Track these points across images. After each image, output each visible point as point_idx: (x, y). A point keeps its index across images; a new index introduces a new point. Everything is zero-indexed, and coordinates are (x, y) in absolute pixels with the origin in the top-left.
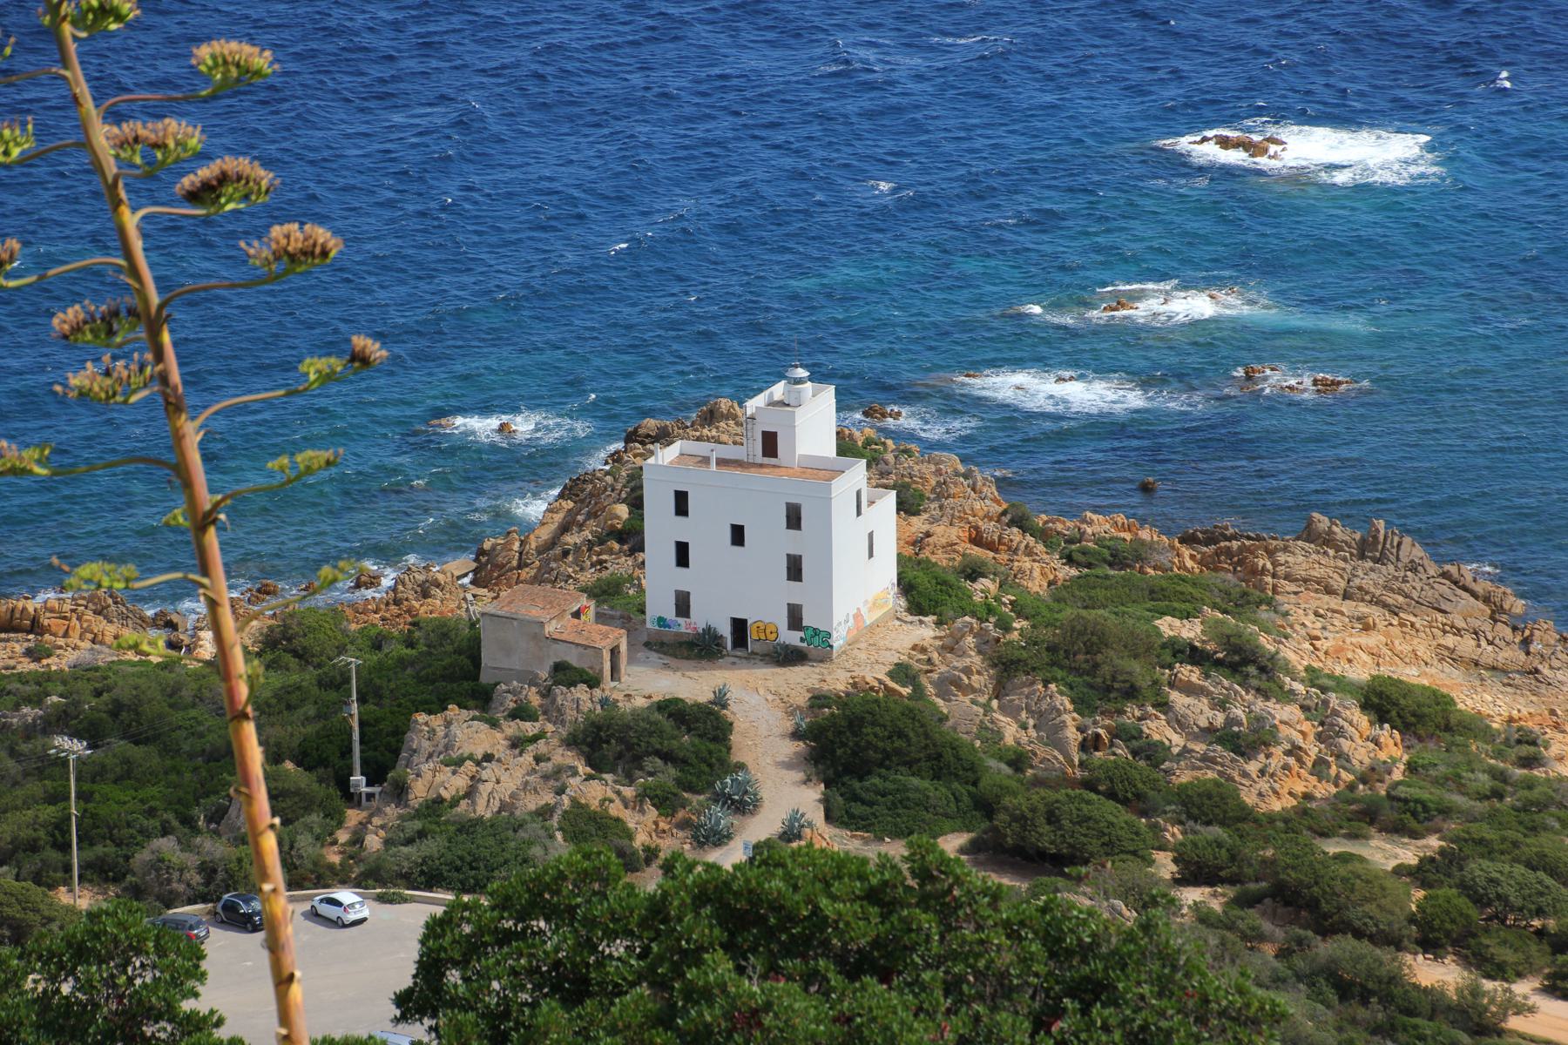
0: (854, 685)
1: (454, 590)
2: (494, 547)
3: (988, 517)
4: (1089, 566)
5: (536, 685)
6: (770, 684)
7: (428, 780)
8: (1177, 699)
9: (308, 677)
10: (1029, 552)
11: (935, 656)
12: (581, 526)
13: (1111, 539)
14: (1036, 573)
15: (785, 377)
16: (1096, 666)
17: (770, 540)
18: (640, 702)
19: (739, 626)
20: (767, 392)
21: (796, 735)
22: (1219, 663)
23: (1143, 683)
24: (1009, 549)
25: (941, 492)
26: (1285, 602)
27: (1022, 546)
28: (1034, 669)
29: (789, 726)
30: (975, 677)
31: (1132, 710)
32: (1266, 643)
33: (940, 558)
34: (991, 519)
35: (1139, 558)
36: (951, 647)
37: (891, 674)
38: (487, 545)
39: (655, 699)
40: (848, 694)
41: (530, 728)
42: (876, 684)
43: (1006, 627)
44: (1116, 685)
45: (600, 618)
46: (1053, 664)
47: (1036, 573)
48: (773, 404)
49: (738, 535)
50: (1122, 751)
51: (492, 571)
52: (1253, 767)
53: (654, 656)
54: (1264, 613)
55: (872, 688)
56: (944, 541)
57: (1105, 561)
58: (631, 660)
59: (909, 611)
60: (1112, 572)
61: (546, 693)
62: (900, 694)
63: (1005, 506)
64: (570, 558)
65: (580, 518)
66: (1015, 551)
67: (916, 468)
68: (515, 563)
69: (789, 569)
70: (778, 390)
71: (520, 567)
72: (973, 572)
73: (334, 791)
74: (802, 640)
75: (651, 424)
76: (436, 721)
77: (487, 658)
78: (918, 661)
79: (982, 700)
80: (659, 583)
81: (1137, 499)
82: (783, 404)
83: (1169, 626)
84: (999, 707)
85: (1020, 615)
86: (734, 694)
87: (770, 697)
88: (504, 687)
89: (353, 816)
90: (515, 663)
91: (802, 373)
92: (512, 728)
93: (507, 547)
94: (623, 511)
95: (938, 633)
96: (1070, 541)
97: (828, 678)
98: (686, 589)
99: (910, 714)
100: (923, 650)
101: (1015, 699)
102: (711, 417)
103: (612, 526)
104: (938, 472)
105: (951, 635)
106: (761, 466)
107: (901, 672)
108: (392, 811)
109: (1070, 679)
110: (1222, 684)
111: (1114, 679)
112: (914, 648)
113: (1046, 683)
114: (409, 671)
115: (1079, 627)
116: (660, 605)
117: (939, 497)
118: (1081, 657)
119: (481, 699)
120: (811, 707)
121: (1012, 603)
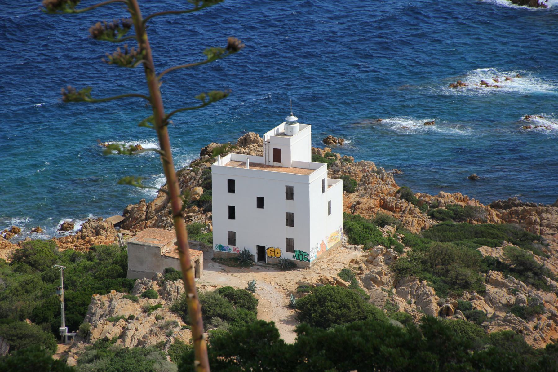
0: (321, 280)
1: (111, 238)
2: (133, 209)
4: (443, 219)
5: (156, 280)
6: (278, 280)
7: (102, 329)
8: (490, 288)
9: (36, 276)
10: (411, 212)
11: (363, 266)
13: (454, 205)
14: (415, 223)
16: (448, 271)
17: (277, 206)
18: (210, 289)
19: (261, 250)
20: (276, 128)
21: (290, 307)
22: (512, 271)
23: (472, 280)
24: (401, 210)
25: (365, 181)
26: (548, 239)
27: (408, 209)
29: (287, 301)
31: (466, 295)
32: (538, 260)
33: (365, 215)
34: (391, 195)
35: (469, 216)
36: (371, 261)
37: (340, 275)
38: (129, 208)
40: (317, 285)
41: (153, 302)
42: (332, 280)
43: (399, 250)
44: (458, 282)
46: (425, 270)
47: (415, 223)
48: (278, 134)
49: (261, 203)
50: (461, 316)
52: (531, 325)
53: (217, 265)
54: (535, 244)
55: (330, 282)
56: (367, 206)
57: (451, 217)
58: (205, 268)
61: (162, 284)
62: (345, 286)
63: (399, 188)
66: (404, 212)
68: (144, 217)
70: (281, 127)
71: (147, 218)
72: (383, 223)
73: (51, 335)
74: (294, 257)
75: (213, 145)
76: (105, 299)
77: (130, 266)
79: (388, 289)
80: (220, 228)
82: (284, 134)
83: (485, 251)
85: (407, 245)
86: (259, 285)
87: (277, 287)
88: (140, 281)
89: (61, 348)
90: (145, 268)
91: (294, 118)
92: (143, 302)
93: (140, 209)
94: (200, 190)
95: (364, 254)
96: (433, 206)
97: (307, 277)
99: (350, 296)
100: (357, 263)
102: (245, 142)
103: (188, 203)
104: (364, 171)
105: (371, 255)
106: (273, 167)
107: (345, 274)
108: (81, 345)
109: (434, 278)
110: (514, 282)
111: (457, 278)
112: (352, 261)
114: (90, 272)
115: (438, 251)
116: (220, 238)
118: (439, 267)
119: (129, 288)
121: (403, 238)
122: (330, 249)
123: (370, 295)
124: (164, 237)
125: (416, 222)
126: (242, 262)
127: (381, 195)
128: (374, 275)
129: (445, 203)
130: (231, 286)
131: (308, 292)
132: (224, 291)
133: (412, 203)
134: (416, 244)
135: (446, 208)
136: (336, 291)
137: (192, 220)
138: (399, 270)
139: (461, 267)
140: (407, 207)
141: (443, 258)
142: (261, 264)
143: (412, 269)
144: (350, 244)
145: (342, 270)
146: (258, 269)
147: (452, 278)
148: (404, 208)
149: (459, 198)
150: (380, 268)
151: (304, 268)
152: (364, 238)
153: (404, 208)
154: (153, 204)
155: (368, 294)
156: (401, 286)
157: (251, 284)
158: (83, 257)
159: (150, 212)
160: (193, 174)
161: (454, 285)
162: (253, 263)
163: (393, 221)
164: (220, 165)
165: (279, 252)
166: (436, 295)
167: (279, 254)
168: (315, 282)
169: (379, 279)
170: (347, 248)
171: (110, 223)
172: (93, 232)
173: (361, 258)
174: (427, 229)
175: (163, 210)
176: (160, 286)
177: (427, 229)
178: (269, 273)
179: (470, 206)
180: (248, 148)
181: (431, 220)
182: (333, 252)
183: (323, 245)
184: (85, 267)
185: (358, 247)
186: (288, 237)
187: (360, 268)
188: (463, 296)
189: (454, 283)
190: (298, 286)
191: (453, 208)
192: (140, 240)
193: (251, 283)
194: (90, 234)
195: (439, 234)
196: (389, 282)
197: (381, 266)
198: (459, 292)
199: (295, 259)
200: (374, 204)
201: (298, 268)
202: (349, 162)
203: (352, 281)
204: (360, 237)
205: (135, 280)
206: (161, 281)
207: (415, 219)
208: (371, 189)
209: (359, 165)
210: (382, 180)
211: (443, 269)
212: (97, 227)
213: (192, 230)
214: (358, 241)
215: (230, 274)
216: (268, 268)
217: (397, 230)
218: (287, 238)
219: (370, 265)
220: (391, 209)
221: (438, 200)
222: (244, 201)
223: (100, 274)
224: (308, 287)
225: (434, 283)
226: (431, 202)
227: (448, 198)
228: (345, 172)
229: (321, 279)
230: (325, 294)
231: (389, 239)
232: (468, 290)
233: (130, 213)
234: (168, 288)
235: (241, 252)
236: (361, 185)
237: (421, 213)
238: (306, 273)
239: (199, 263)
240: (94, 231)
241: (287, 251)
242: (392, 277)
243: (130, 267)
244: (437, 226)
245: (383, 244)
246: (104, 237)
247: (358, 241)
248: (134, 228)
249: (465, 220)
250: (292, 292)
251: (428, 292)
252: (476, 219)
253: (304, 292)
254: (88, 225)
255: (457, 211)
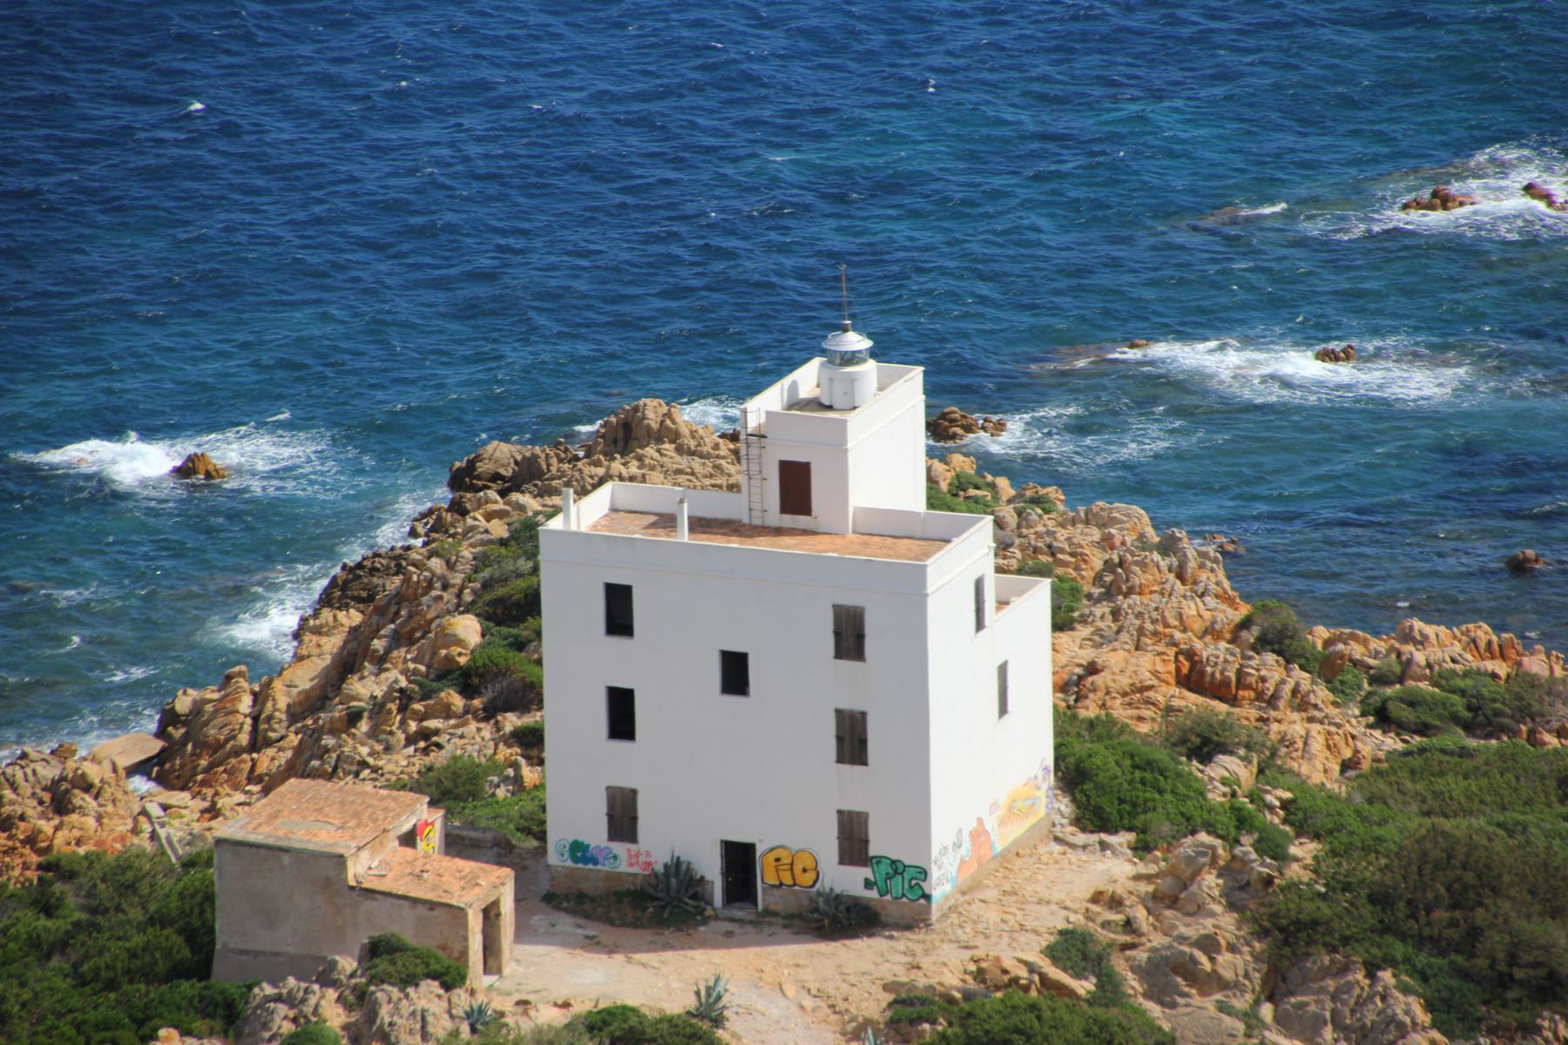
0: (980, 975)
2: (198, 708)
3: (1211, 631)
4: (1423, 729)
5: (334, 984)
6: (807, 975)
10: (1301, 703)
11: (1140, 914)
12: (381, 661)
13: (1466, 675)
14: (1317, 745)
15: (823, 352)
16: (1474, 933)
17: (801, 683)
18: (548, 1016)
19: (739, 858)
20: (786, 382)
24: (1260, 696)
25: (1114, 583)
27: (1287, 690)
28: (1346, 940)
30: (1224, 958)
34: (1218, 636)
35: (1525, 712)
36: (1172, 896)
37: (1052, 953)
38: (183, 704)
39: (581, 1007)
40: (968, 996)
42: (1023, 973)
43: (1272, 848)
44: (1519, 974)
45: (455, 845)
46: (1385, 929)
47: (1317, 745)
48: (796, 404)
49: (735, 674)
51: (196, 755)
53: (565, 923)
55: (1015, 981)
56: (1125, 681)
57: (1455, 719)
58: (524, 933)
59: (1079, 823)
60: (1472, 743)
61: (361, 1000)
62: (1071, 993)
63: (1244, 610)
64: (364, 726)
65: (378, 645)
66: (1272, 701)
67: (1062, 534)
68: (244, 739)
69: (840, 739)
70: (807, 378)
71: (256, 745)
72: (1206, 746)
74: (868, 884)
75: (502, 454)
77: (227, 933)
78: (1106, 925)
79: (1241, 1003)
80: (574, 781)
81: (1504, 587)
82: (817, 404)
84: (1278, 1019)
85: (1303, 829)
86: (736, 996)
87: (809, 1003)
88: (269, 990)
90: (284, 939)
91: (855, 341)
93: (225, 707)
95: (1142, 868)
96: (1380, 679)
97: (925, 962)
98: (628, 784)
100: (1115, 903)
101: (1308, 1001)
104: (1107, 542)
105: (1172, 872)
106: (778, 531)
107: (1073, 948)
109: (1422, 959)
111: (1513, 960)
112: (1096, 898)
113: (1371, 971)
114: (55, 961)
115: (1437, 854)
116: (574, 817)
117: (1110, 593)
118: (1441, 915)
120: (893, 1023)
121: (1285, 805)
122: (1007, 850)
123: (1174, 1029)
124: (356, 815)
125: (1321, 739)
126: (661, 906)
127: (1178, 635)
128: (1186, 949)
129: (1429, 666)
130: (631, 1002)
131: (933, 1022)
132: (605, 1023)
133: (1302, 668)
134: (1340, 828)
135: (1436, 685)
136: (1047, 1014)
137: (439, 746)
138: (1282, 929)
139: (1529, 917)
140: (1283, 682)
141: (1458, 879)
142: (738, 914)
143: (1336, 924)
144: (1084, 830)
145: (1061, 933)
146: (729, 934)
147: (1494, 960)
148: (1270, 687)
149: (1482, 645)
150: (1209, 922)
151: (909, 927)
152: (1135, 805)
153: (1270, 687)
154: (278, 685)
155: (1166, 1027)
156: (1292, 994)
157: (709, 995)
158: (20, 900)
159: (270, 718)
160: (436, 564)
161: (1505, 987)
162: (709, 912)
163: (1244, 739)
164: (573, 528)
165: (810, 864)
166: (1435, 1025)
167: (810, 876)
168: (956, 982)
169: (1207, 966)
170: (1073, 846)
171: (107, 765)
172: (41, 803)
173: (1131, 885)
174: (1366, 766)
175: (322, 708)
176: (348, 1007)
177: (1366, 766)
178: (770, 949)
179: (1527, 674)
180: (640, 458)
181: (1377, 733)
182: (1019, 862)
183: (979, 834)
184: (34, 942)
185: (1113, 839)
186: (846, 807)
187: (1128, 925)
188: (1538, 1030)
189: (1505, 980)
190: (891, 997)
191: (1460, 683)
192: (265, 829)
193: (709, 990)
194: (31, 809)
195: (1419, 787)
196: (1247, 976)
197: (1213, 914)
198: (1526, 1016)
199: (873, 894)
200: (1155, 674)
201: (885, 926)
202: (1047, 511)
203: (1098, 976)
204: (1121, 801)
205: (250, 988)
206: (354, 989)
207: (1315, 727)
208: (1139, 615)
209: (1087, 522)
210: (1181, 576)
211: (1454, 923)
212: (55, 783)
213: (448, 784)
214: (1115, 817)
215: (619, 958)
216: (767, 930)
217: (1261, 771)
218: (840, 812)
219: (1168, 913)
220: (1220, 691)
221: (1399, 655)
222: (667, 666)
223: (97, 970)
224: (932, 1003)
225: (1425, 979)
226: (1372, 662)
227: (1441, 645)
228: (1036, 550)
229: (981, 971)
230: (1005, 1029)
231: (1232, 808)
232: (1557, 1005)
233: (184, 724)
234: (384, 1014)
235: (659, 868)
236: (1098, 601)
237: (1335, 704)
238: (918, 948)
239: (498, 915)
240: (47, 797)
241: (841, 862)
242: (1257, 958)
243: (225, 935)
244: (1407, 754)
245: (1211, 830)
246: (91, 822)
247: (1115, 817)
248: (204, 783)
249: (1515, 733)
250: (868, 1022)
251: (1401, 1016)
252: (1555, 725)
253: (915, 1021)
254: (19, 775)
255: (1479, 696)
